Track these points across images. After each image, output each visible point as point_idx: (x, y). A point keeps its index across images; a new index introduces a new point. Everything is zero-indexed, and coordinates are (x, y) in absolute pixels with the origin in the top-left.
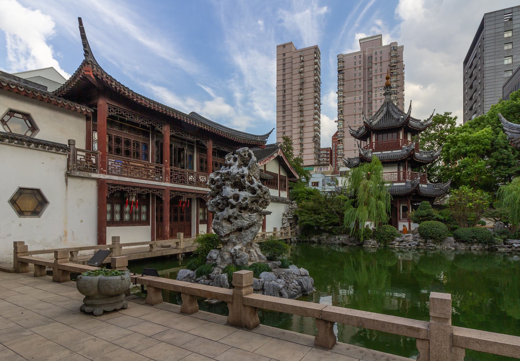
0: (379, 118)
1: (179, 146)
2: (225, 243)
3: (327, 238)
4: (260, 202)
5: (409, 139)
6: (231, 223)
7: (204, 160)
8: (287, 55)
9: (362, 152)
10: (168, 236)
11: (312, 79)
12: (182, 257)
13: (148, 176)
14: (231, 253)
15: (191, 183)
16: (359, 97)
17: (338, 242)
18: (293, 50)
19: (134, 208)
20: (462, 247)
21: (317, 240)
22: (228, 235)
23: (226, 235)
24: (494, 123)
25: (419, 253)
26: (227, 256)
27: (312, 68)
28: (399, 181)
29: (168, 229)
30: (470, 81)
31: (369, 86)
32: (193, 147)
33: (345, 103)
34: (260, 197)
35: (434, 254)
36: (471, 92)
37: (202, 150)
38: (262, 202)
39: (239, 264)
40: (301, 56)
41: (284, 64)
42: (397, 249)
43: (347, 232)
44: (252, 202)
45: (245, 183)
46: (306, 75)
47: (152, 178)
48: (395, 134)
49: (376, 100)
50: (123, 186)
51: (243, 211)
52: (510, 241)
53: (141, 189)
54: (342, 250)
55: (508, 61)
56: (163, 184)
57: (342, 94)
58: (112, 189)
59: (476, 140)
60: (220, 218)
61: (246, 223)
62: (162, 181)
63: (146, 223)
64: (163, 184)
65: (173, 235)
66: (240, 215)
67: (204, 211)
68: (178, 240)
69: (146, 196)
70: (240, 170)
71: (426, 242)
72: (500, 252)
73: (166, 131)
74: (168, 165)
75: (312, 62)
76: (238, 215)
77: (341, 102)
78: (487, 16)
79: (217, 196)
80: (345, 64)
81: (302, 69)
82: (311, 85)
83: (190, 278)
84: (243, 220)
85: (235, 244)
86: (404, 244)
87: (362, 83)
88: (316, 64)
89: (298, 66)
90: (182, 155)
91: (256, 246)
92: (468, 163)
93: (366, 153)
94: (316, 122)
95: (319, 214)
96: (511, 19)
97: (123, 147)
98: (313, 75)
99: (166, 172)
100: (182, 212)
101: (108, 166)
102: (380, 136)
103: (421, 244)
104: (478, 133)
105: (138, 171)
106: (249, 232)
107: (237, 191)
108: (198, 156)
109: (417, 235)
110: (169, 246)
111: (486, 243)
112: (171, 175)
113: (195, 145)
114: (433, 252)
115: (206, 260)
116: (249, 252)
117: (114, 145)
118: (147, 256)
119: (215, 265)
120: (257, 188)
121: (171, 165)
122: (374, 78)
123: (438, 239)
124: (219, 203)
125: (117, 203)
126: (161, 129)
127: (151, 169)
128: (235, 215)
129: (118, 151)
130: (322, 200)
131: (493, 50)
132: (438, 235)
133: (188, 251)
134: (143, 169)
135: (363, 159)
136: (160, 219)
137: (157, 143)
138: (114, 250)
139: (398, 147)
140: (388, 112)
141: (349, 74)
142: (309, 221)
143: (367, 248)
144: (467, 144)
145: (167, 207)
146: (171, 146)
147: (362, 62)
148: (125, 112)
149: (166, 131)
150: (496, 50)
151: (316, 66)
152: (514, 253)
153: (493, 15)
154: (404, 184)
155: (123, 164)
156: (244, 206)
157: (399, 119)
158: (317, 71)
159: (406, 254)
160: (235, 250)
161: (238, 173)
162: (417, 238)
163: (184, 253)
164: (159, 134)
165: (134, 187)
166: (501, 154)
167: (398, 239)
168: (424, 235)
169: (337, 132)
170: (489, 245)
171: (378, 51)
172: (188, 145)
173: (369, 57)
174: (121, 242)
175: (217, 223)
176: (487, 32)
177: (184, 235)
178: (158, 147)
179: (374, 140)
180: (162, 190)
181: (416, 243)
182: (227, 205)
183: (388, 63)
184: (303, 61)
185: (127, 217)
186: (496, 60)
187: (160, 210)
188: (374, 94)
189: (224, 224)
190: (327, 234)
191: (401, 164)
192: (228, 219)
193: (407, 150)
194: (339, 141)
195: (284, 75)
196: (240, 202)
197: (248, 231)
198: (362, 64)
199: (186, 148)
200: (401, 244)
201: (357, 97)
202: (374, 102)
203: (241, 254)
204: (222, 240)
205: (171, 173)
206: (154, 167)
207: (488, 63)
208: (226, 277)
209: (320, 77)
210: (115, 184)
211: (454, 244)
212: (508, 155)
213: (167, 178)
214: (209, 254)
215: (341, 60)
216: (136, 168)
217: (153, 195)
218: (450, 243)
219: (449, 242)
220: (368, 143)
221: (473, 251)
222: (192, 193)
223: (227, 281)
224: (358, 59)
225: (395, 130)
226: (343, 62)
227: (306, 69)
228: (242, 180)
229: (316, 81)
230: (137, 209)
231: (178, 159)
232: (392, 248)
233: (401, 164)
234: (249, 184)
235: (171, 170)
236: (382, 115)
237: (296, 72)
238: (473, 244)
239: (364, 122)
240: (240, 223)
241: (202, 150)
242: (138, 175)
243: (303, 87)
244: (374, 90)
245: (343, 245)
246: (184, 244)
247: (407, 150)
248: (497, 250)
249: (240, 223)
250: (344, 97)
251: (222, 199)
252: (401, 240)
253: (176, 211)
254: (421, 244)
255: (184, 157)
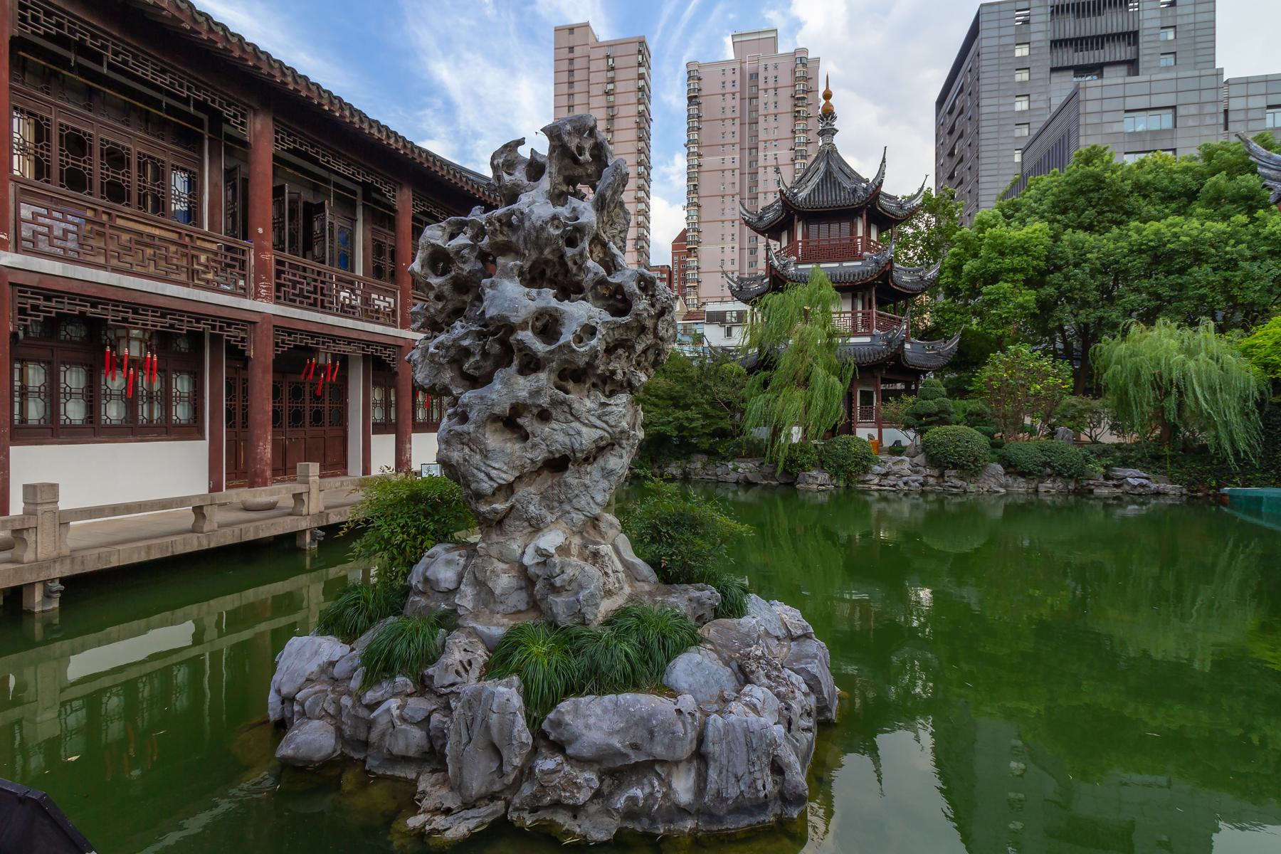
0: (811, 185)
1: (307, 196)
2: (495, 524)
3: (704, 468)
4: (639, 348)
5: (874, 236)
6: (524, 436)
7: (388, 249)
8: (578, 52)
9: (776, 263)
10: (269, 473)
11: (633, 110)
12: (313, 539)
13: (193, 274)
14: (523, 569)
15: (346, 311)
16: (732, 158)
17: (733, 477)
18: (591, 40)
19: (143, 383)
20: (1020, 486)
21: (679, 471)
22: (509, 489)
23: (500, 487)
24: (1044, 211)
25: (926, 502)
26: (504, 581)
27: (632, 86)
28: (855, 333)
29: (266, 450)
30: (949, 141)
31: (750, 137)
32: (352, 205)
33: (702, 169)
34: (642, 330)
35: (960, 504)
36: (950, 164)
37: (383, 217)
38: (645, 352)
39: (563, 618)
40: (608, 57)
41: (571, 71)
42: (876, 494)
43: (755, 451)
44: (609, 350)
45: (581, 268)
46: (620, 99)
47: (208, 281)
48: (846, 226)
49: (765, 167)
50: (84, 298)
51: (570, 385)
52: (1120, 472)
53: (163, 316)
54: (742, 496)
55: (1021, 105)
56: (247, 304)
57: (695, 149)
58: (35, 308)
59: (1022, 247)
60: (473, 415)
61: (589, 436)
62: (245, 296)
63: (191, 430)
64: (247, 304)
65: (283, 469)
66: (563, 402)
67: (387, 395)
68: (300, 488)
69: (186, 343)
70: (564, 211)
71: (942, 475)
72: (1097, 498)
73: (261, 133)
74: (268, 244)
75: (633, 73)
76: (555, 403)
77: (693, 166)
78: (985, 10)
79: (458, 324)
80: (703, 84)
81: (610, 87)
82: (631, 123)
83: (334, 680)
84: (576, 425)
85: (536, 527)
86: (891, 480)
87: (737, 128)
88: (641, 77)
89: (601, 77)
90: (316, 225)
91: (612, 525)
92: (1004, 294)
93: (785, 266)
94: (642, 206)
95: (686, 407)
96: (1026, 22)
97: (97, 168)
98: (635, 101)
99: (261, 265)
100: (317, 398)
101: (18, 220)
102: (813, 228)
103: (931, 480)
104: (1015, 234)
105: (149, 251)
106: (597, 475)
107: (548, 298)
108: (370, 236)
109: (920, 459)
110: (272, 507)
111: (1071, 477)
112: (278, 277)
113: (360, 202)
114: (959, 500)
115: (407, 591)
116: (596, 555)
117: (56, 156)
118: (180, 550)
119: (449, 621)
120: (633, 286)
121: (279, 246)
122: (761, 119)
123: (969, 467)
124: (467, 352)
125: (72, 363)
126: (242, 124)
127: (205, 250)
128: (544, 401)
129: (76, 180)
130: (695, 373)
131: (996, 80)
132: (972, 459)
133: (334, 519)
134: (173, 248)
135: (778, 281)
136: (238, 419)
137: (230, 174)
138: (30, 537)
139: (854, 256)
140: (828, 174)
141: (711, 106)
142: (663, 424)
143: (807, 491)
144: (1002, 254)
145: (262, 381)
146: (278, 192)
147: (738, 84)
148: (94, 36)
149: (261, 133)
150: (1002, 80)
151: (641, 83)
152: (1126, 498)
153: (996, 8)
154: (868, 340)
155: (88, 221)
156: (582, 362)
157: (855, 190)
158: (643, 93)
159: (895, 506)
160: (539, 552)
161: (555, 217)
162: (918, 465)
163: (320, 528)
164: (238, 148)
165: (136, 308)
166: (1067, 278)
167: (877, 469)
168: (938, 460)
169: (685, 231)
170: (1077, 481)
171: (771, 63)
172: (338, 198)
173: (751, 75)
174: (63, 505)
175: (459, 435)
176: (986, 41)
177: (323, 468)
178: (234, 187)
179: (799, 237)
180: (247, 323)
181: (921, 479)
182: (504, 359)
183: (790, 91)
184: (613, 69)
185: (113, 412)
186: (1002, 101)
187: (238, 388)
188: (761, 154)
189: (494, 440)
190: (705, 458)
191: (860, 294)
192: (510, 422)
193: (877, 262)
194: (690, 250)
195: (571, 95)
196: (567, 346)
197: (594, 470)
198: (737, 88)
199: (329, 204)
200: (885, 482)
201: (728, 158)
202: (761, 171)
203: (570, 572)
204: (484, 508)
205: (279, 274)
206: (214, 247)
207: (988, 105)
208: (517, 701)
209: (651, 107)
210: (46, 291)
211: (1003, 480)
212: (1082, 284)
213: (262, 285)
214: (419, 568)
215: (693, 75)
216: (142, 241)
217: (216, 339)
218: (994, 480)
219: (993, 476)
220: (785, 244)
221: (1042, 496)
222: (350, 341)
223: (521, 721)
224: (729, 77)
225: (845, 214)
226: (699, 79)
227: (620, 87)
228: (570, 252)
229: (641, 114)
230: (156, 386)
231: (301, 231)
232: (865, 492)
233: (860, 294)
234: (602, 271)
235: (279, 262)
236: (816, 180)
237: (597, 90)
238: (1042, 479)
239: (781, 191)
240: (561, 437)
241: (383, 217)
242: (152, 269)
243: (612, 125)
244: (761, 145)
245: (748, 484)
246: (320, 497)
247: (877, 262)
248: (1091, 491)
249: (561, 437)
250: (700, 155)
251: (481, 336)
252: (884, 471)
253: (297, 393)
254: (931, 480)
255: (323, 229)
